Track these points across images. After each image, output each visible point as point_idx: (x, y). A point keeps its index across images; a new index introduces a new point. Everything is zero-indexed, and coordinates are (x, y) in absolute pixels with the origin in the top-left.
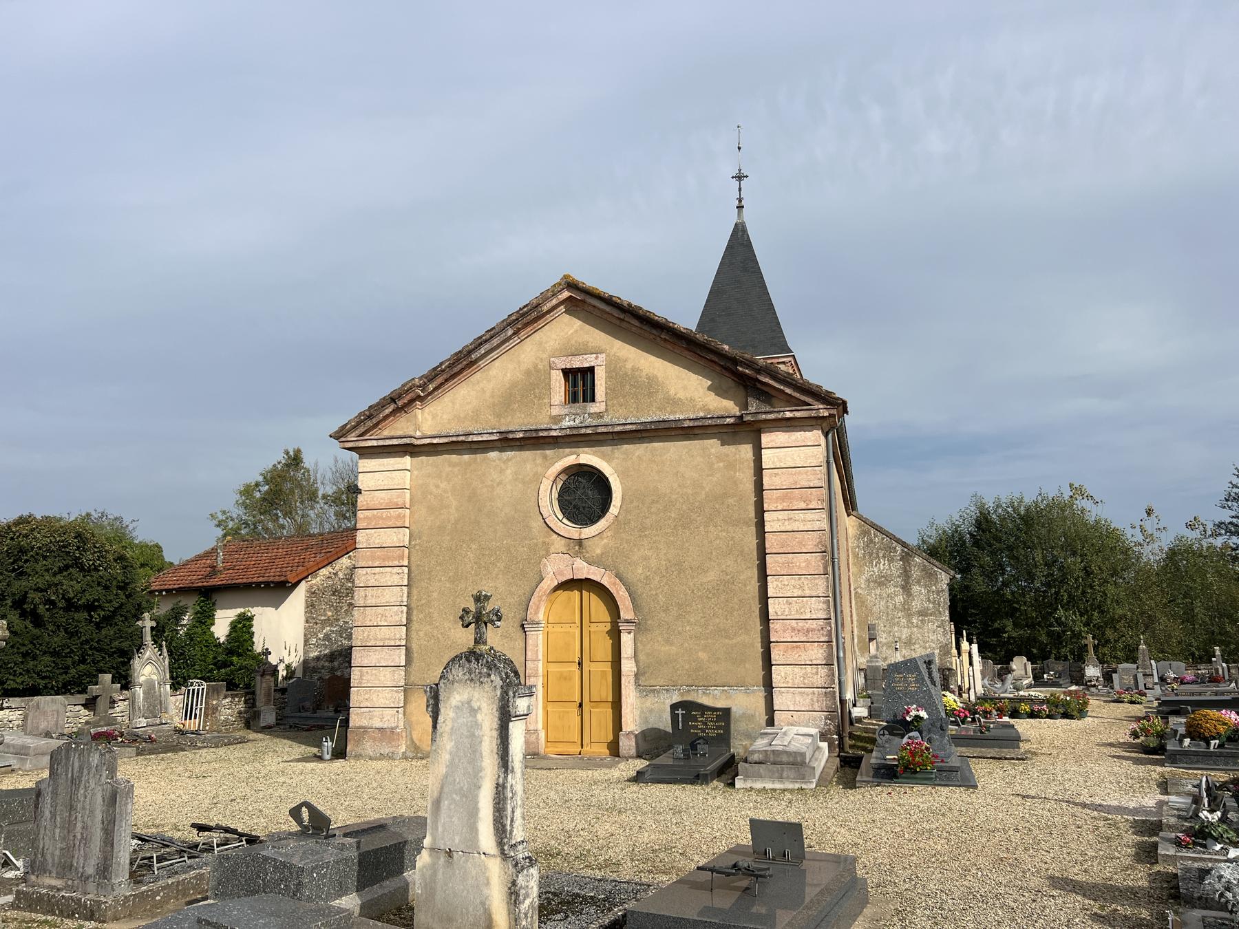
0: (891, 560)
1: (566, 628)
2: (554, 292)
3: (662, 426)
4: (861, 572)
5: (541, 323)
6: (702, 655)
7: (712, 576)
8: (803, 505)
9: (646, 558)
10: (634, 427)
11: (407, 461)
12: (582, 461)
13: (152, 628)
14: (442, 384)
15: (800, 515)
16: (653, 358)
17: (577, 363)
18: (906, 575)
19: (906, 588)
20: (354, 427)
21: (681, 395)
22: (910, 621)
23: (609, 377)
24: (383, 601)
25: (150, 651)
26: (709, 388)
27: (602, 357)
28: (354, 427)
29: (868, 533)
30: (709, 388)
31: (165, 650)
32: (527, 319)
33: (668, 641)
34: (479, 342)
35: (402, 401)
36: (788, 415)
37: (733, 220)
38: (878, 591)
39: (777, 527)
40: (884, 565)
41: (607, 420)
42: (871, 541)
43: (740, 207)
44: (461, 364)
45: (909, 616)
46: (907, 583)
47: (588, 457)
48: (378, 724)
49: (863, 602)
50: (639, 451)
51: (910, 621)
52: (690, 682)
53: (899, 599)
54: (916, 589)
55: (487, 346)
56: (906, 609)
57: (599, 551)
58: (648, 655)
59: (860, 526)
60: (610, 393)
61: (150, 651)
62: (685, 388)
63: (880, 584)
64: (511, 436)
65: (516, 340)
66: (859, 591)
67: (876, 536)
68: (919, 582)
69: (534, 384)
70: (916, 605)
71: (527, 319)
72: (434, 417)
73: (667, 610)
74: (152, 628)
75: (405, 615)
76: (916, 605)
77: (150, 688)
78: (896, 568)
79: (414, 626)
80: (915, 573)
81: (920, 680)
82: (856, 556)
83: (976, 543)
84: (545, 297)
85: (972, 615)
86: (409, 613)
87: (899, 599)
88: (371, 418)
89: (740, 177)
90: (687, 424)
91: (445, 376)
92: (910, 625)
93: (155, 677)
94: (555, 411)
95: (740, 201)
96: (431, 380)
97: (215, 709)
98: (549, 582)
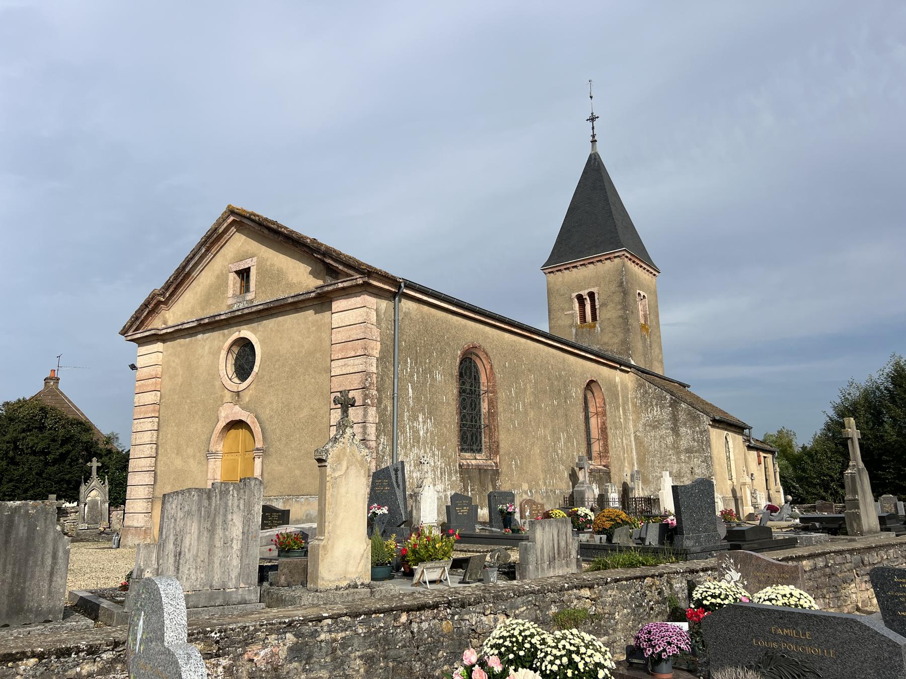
1: (234, 456)
2: (223, 219)
3: (277, 304)
5: (223, 241)
6: (297, 472)
7: (304, 414)
8: (353, 354)
9: (271, 403)
10: (261, 307)
11: (159, 346)
12: (242, 336)
13: (98, 467)
14: (194, 255)
15: (351, 361)
16: (281, 256)
17: (243, 266)
18: (675, 419)
19: (675, 430)
20: (131, 326)
21: (295, 281)
22: (679, 458)
23: (258, 273)
24: (142, 441)
25: (95, 481)
26: (310, 273)
27: (255, 259)
28: (131, 326)
29: (644, 385)
30: (310, 273)
31: (107, 481)
32: (213, 240)
33: (280, 463)
34: (188, 261)
35: (153, 305)
36: (340, 285)
37: (588, 152)
38: (653, 434)
39: (338, 372)
40: (656, 411)
41: (255, 303)
42: (646, 392)
43: (594, 142)
44: (181, 279)
45: (678, 453)
46: (675, 425)
47: (245, 332)
48: (136, 525)
50: (270, 324)
51: (679, 458)
52: (290, 493)
53: (670, 440)
54: (683, 430)
55: (193, 262)
56: (675, 447)
57: (247, 399)
58: (269, 473)
59: (637, 380)
60: (259, 284)
61: (95, 481)
62: (297, 274)
63: (655, 428)
64: (202, 322)
65: (210, 256)
66: (638, 434)
67: (650, 388)
68: (685, 424)
69: (220, 285)
70: (684, 444)
71: (213, 240)
72: (174, 313)
73: (280, 440)
74: (98, 467)
75: (154, 450)
76: (684, 444)
77: (94, 503)
78: (667, 412)
79: (159, 457)
80: (682, 416)
81: (390, 484)
82: (634, 405)
83: (893, 399)
84: (219, 223)
85: (887, 462)
86: (157, 449)
88: (139, 319)
89: (593, 119)
90: (290, 300)
91: (174, 286)
92: (679, 461)
93: (99, 498)
94: (230, 302)
95: (593, 136)
96: (167, 290)
98: (222, 424)
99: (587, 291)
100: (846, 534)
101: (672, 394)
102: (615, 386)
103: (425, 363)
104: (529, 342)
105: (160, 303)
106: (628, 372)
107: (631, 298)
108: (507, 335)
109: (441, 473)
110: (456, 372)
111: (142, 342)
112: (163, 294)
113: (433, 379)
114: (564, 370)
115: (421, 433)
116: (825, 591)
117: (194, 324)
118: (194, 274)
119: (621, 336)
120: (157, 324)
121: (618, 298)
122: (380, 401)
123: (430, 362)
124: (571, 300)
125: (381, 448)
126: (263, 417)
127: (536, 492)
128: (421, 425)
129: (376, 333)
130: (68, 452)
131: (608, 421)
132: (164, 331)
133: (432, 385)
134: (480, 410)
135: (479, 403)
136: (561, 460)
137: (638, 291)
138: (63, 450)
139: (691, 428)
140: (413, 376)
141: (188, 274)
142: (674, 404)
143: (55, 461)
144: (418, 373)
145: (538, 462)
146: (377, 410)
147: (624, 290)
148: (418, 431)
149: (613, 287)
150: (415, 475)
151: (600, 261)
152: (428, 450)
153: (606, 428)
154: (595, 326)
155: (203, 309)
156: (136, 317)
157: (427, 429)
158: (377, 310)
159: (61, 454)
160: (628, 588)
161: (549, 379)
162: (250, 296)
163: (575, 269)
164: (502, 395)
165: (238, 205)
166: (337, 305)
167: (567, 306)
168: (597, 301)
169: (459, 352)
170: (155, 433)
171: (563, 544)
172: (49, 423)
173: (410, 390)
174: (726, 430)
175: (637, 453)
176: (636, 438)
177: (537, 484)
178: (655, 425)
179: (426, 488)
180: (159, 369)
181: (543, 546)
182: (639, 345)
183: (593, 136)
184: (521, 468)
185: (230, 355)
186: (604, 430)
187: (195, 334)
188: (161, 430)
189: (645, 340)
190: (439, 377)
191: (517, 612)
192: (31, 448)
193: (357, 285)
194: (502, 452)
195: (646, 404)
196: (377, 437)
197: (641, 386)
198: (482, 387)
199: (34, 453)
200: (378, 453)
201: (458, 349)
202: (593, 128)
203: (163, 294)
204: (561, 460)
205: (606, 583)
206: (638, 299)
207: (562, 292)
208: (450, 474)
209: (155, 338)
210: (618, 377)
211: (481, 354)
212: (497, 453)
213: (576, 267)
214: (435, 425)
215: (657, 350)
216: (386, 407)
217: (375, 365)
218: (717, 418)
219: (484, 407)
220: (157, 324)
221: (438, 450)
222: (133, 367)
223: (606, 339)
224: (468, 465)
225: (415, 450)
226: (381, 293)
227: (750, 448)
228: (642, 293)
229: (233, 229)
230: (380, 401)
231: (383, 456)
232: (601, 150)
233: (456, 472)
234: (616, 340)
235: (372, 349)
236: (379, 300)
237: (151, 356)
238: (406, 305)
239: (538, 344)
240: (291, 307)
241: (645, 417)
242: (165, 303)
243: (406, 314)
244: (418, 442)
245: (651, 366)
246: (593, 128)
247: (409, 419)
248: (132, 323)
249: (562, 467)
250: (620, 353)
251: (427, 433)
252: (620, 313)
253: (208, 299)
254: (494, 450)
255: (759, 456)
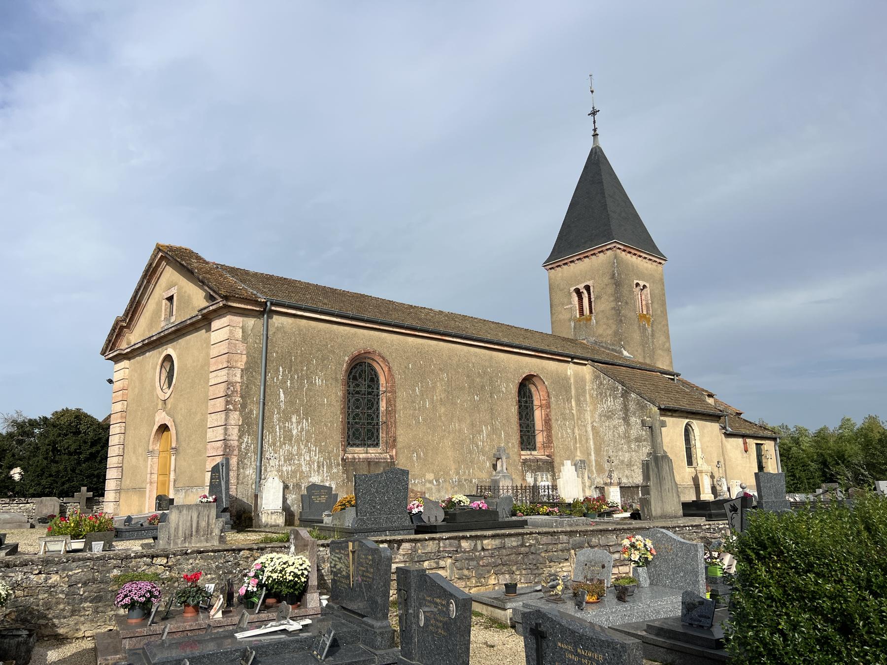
0: (615, 398)
2: (155, 256)
4: (595, 409)
5: (158, 273)
14: (140, 287)
16: (191, 284)
18: (626, 409)
19: (626, 420)
20: (107, 348)
22: (629, 447)
28: (107, 348)
34: (137, 292)
35: (119, 330)
40: (610, 402)
42: (601, 383)
43: (595, 135)
46: (626, 415)
47: (170, 350)
49: (597, 433)
50: (182, 341)
51: (629, 447)
54: (633, 419)
56: (626, 436)
59: (594, 372)
63: (609, 418)
65: (151, 286)
66: (595, 424)
67: (604, 379)
68: (634, 414)
69: (157, 313)
71: (150, 274)
80: (632, 406)
82: (591, 396)
87: (622, 429)
88: (111, 343)
89: (594, 113)
90: (189, 322)
95: (595, 130)
97: (194, 362)
98: (156, 427)
99: (583, 285)
100: (640, 519)
101: (623, 384)
102: (567, 379)
103: (302, 370)
104: (441, 343)
105: (122, 328)
106: (585, 365)
107: (625, 291)
108: (411, 339)
109: (319, 467)
110: (341, 375)
111: (117, 359)
112: (124, 320)
113: (311, 383)
114: (491, 366)
115: (294, 432)
116: (514, 568)
117: (140, 345)
118: (144, 302)
119: (614, 327)
120: (123, 347)
121: (610, 290)
122: (244, 406)
123: (307, 370)
124: (570, 294)
125: (244, 446)
126: (178, 421)
127: (445, 481)
128: (295, 425)
129: (241, 347)
130: (98, 452)
131: (553, 413)
132: (128, 350)
133: (308, 389)
134: (378, 409)
135: (378, 403)
136: (482, 452)
137: (635, 282)
138: (94, 450)
139: (640, 417)
140: (286, 382)
141: (139, 303)
142: (625, 395)
143: (87, 460)
144: (292, 379)
145: (450, 454)
146: (241, 414)
147: (619, 282)
148: (290, 431)
149: (607, 280)
150: (284, 469)
151: (594, 254)
152: (302, 447)
153: (550, 420)
154: (591, 319)
155: (149, 331)
156: (109, 341)
157: (302, 428)
158: (243, 328)
159: (91, 454)
160: (220, 557)
161: (468, 376)
162: (173, 319)
163: (572, 264)
164: (402, 395)
165: (166, 242)
166: (215, 324)
167: (566, 300)
168: (592, 294)
169: (347, 358)
170: (122, 436)
171: (203, 524)
172: (82, 428)
173: (282, 395)
174: (687, 418)
175: (595, 444)
176: (593, 428)
177: (448, 474)
178: (608, 415)
179: (270, 480)
180: (126, 382)
181: (178, 525)
182: (637, 336)
183: (595, 130)
184: (425, 460)
185: (163, 370)
186: (547, 422)
187: (144, 353)
188: (127, 432)
189: (645, 329)
190: (318, 382)
191: (70, 573)
192: (68, 448)
193: (220, 308)
194: (399, 445)
195: (602, 395)
196: (240, 437)
197: (597, 377)
198: (381, 389)
199: (70, 454)
200: (240, 450)
201: (345, 355)
202: (594, 122)
203: (124, 320)
204: (482, 452)
205: (186, 554)
206: (637, 290)
207: (562, 287)
208: (330, 467)
209: (121, 357)
210: (570, 369)
211: (380, 360)
212: (394, 446)
213: (573, 262)
214: (313, 425)
215: (662, 339)
216: (251, 411)
217: (239, 375)
218: (663, 407)
219: (383, 406)
220: (123, 347)
221: (316, 446)
222: (110, 381)
223: (600, 331)
224: (354, 458)
225: (287, 447)
226: (246, 312)
227: (728, 435)
228: (642, 283)
229: (164, 263)
230: (244, 406)
231: (246, 453)
232: (603, 143)
233: (338, 465)
234: (610, 332)
235: (236, 361)
236: (245, 319)
237: (122, 371)
238: (277, 320)
239: (453, 345)
240: (191, 328)
241: (602, 408)
242: (128, 327)
243: (278, 329)
244: (291, 440)
245: (652, 357)
246: (594, 122)
247: (279, 421)
248: (107, 345)
249: (482, 458)
250: (613, 344)
251: (301, 432)
252: (613, 305)
253: (151, 325)
254: (392, 443)
255: (745, 443)
